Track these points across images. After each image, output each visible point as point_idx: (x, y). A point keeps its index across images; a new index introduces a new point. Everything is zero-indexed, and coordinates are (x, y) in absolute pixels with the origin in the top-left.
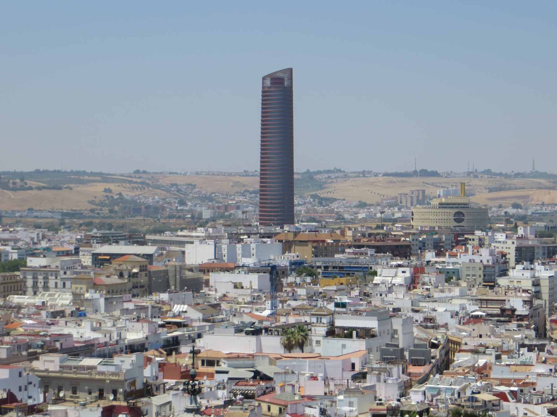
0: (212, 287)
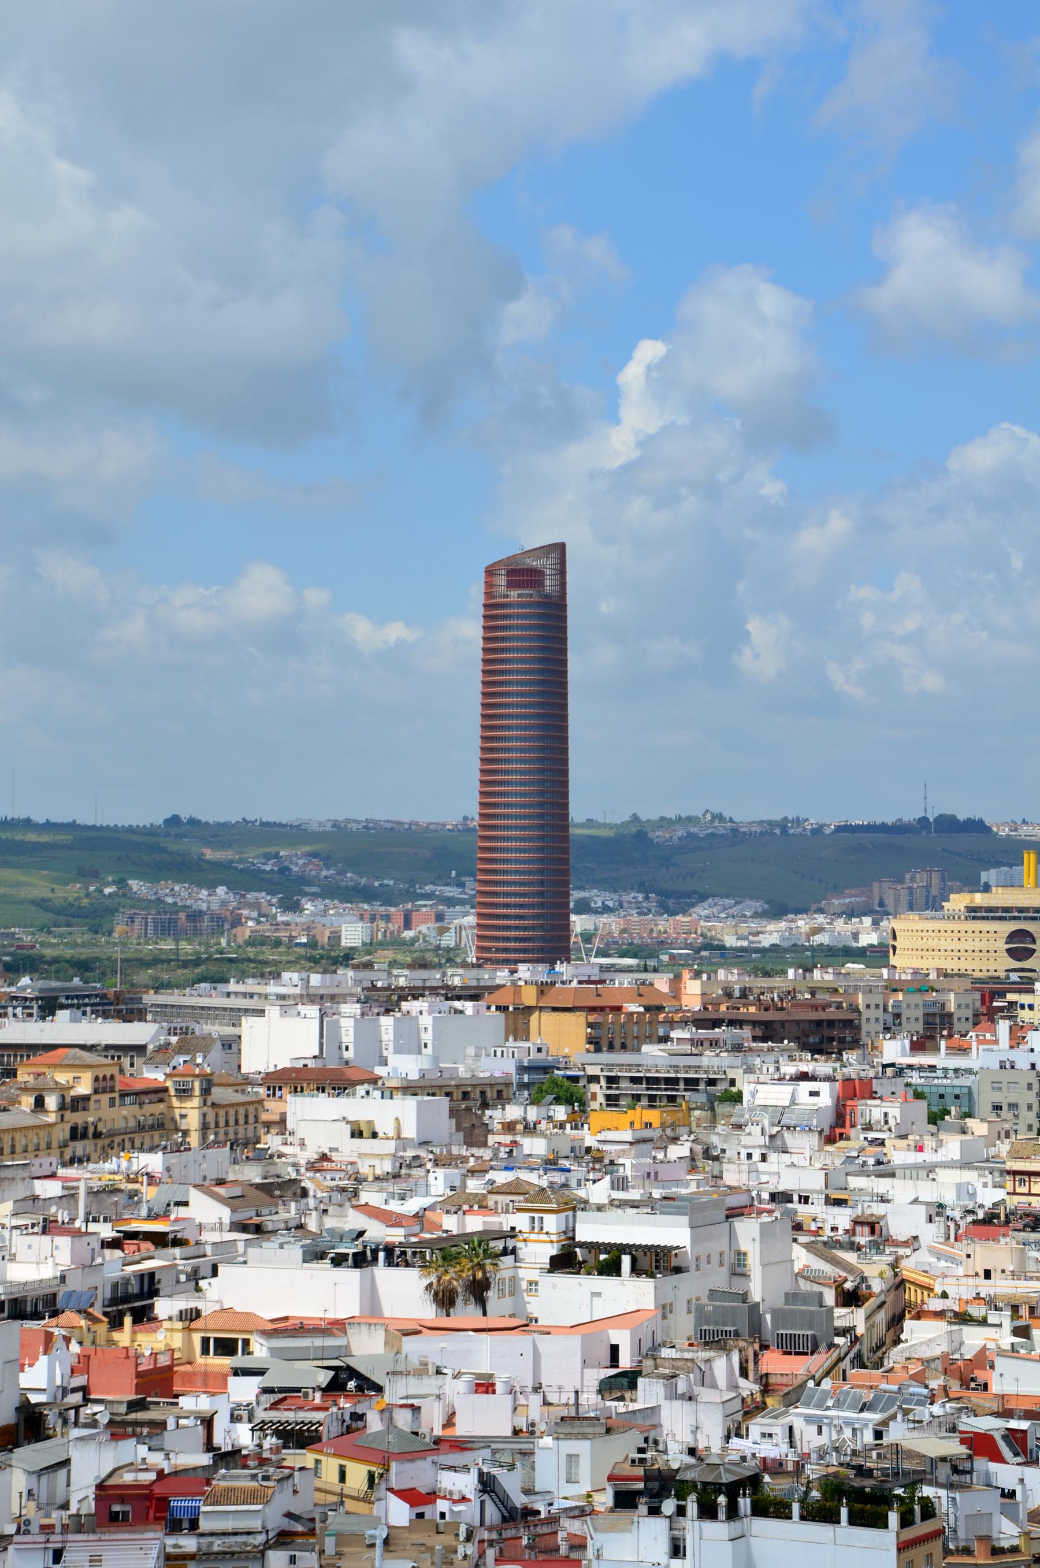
0: (292, 1133)
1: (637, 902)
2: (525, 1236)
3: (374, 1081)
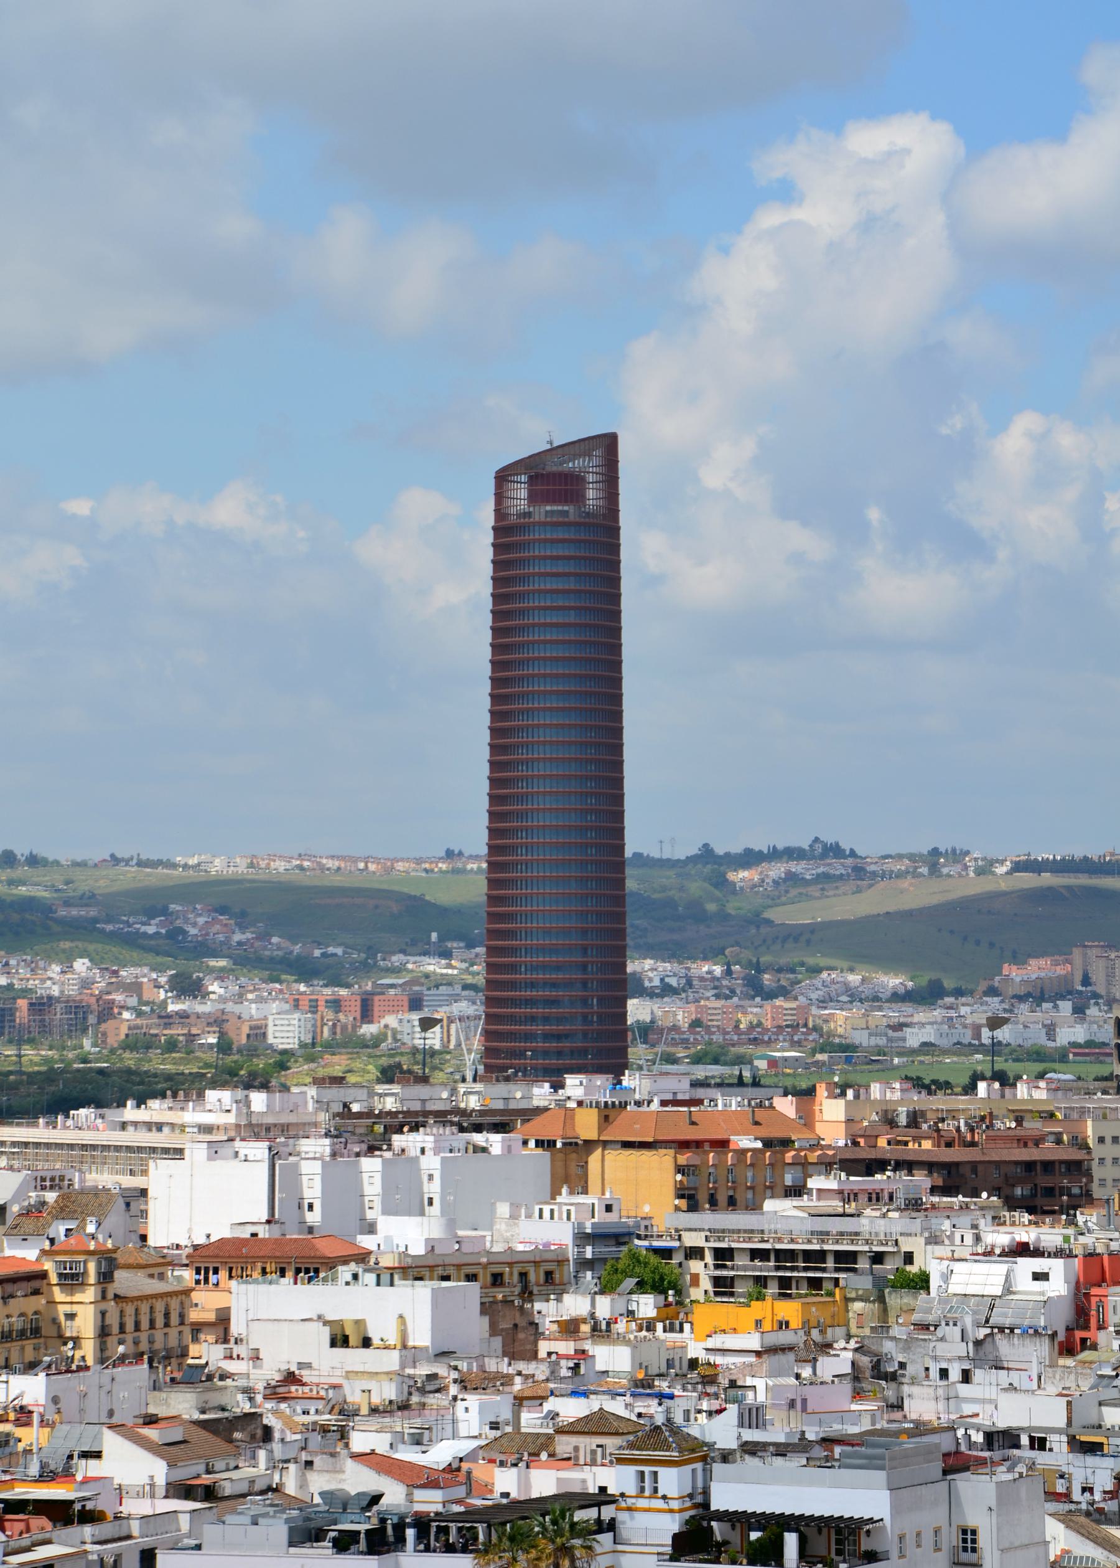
1: (714, 979)
2: (630, 1501)
3: (362, 1257)
